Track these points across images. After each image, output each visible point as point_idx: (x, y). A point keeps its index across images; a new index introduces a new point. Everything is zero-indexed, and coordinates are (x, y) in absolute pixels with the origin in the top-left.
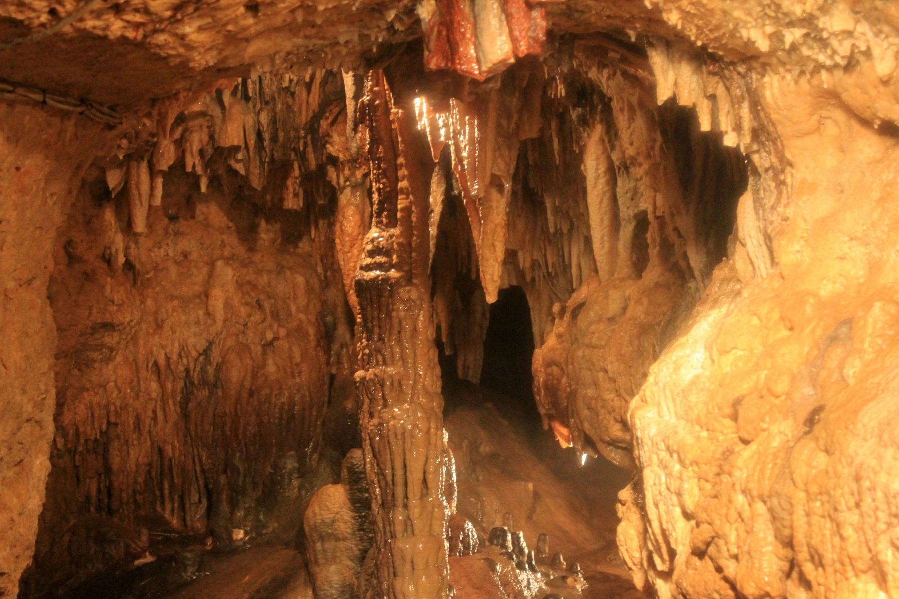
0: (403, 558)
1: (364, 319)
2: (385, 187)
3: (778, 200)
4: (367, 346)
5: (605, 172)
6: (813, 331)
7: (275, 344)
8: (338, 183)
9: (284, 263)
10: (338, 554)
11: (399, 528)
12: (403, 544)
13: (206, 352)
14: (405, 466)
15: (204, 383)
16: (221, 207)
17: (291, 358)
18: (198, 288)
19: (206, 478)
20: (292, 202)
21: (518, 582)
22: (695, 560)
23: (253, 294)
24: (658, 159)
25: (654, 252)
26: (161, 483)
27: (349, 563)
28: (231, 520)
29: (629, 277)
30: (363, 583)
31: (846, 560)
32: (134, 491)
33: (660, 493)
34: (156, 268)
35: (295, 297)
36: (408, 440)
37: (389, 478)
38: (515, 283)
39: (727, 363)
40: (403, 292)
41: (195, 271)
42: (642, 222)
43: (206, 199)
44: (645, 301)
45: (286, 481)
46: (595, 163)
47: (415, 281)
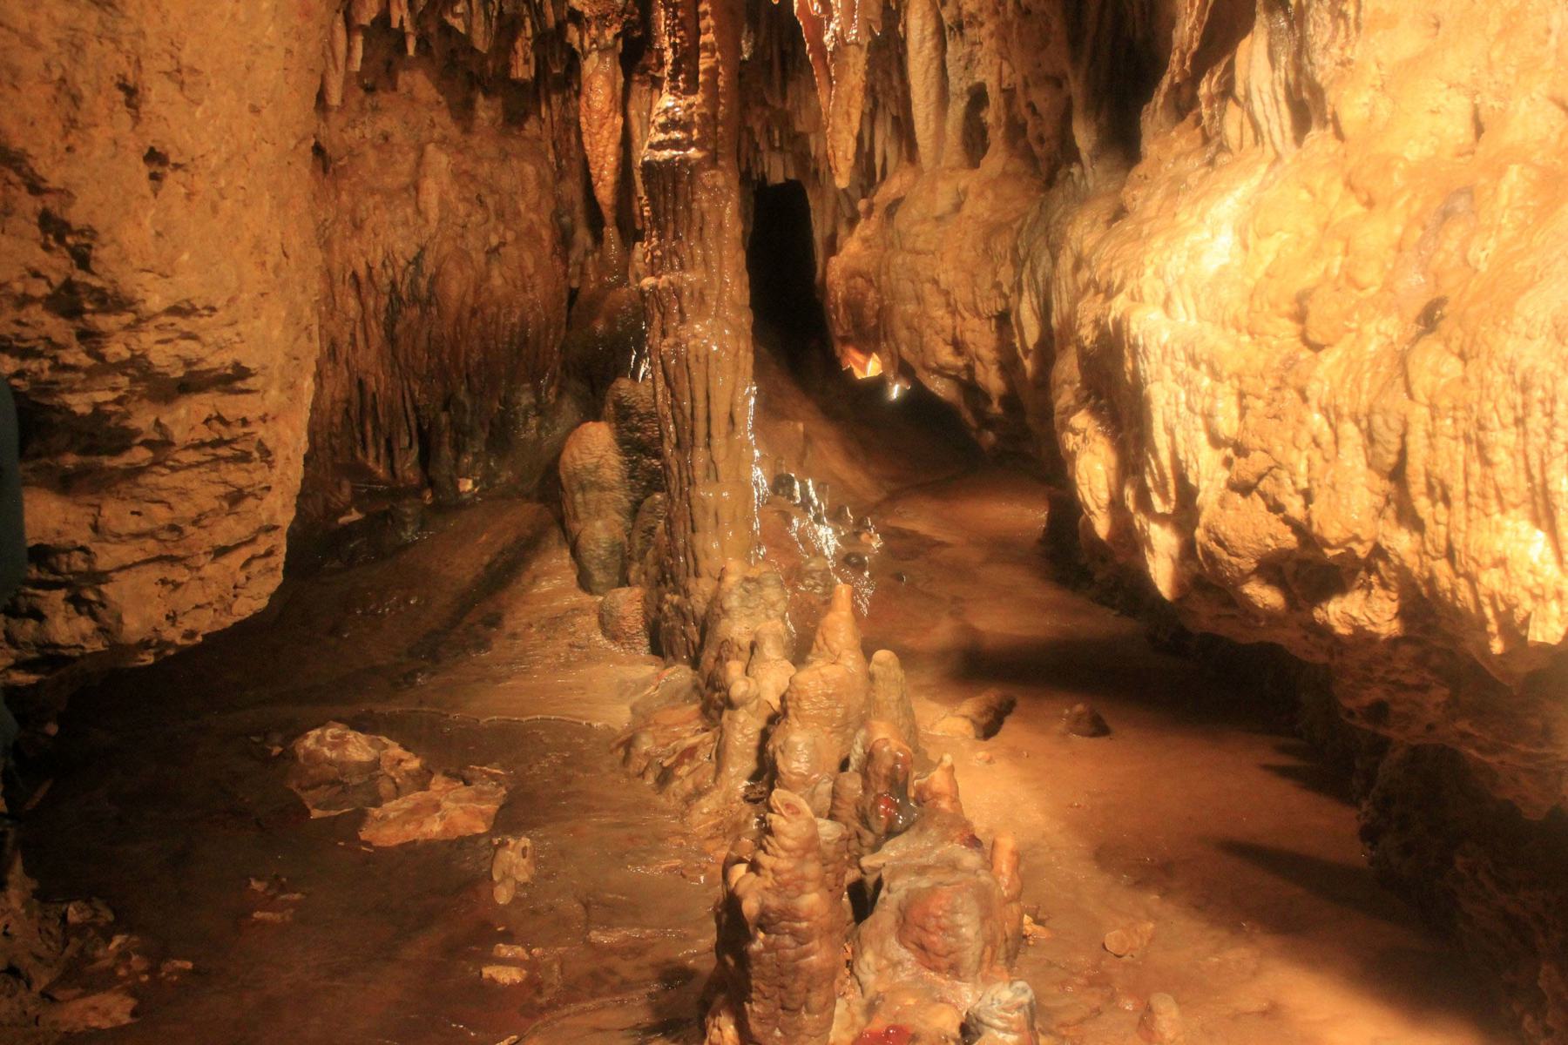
0: (705, 511)
1: (654, 211)
2: (683, 42)
3: (1333, 38)
4: (658, 247)
5: (934, 34)
6: (1408, 204)
7: (502, 250)
8: (582, 46)
9: (508, 148)
10: (604, 506)
11: (699, 473)
12: (705, 493)
13: (417, 261)
14: (708, 397)
15: (415, 299)
16: (428, 75)
17: (522, 268)
18: (405, 180)
19: (418, 418)
20: (522, 71)
21: (819, 538)
22: (1237, 497)
23: (472, 187)
24: (1010, 15)
25: (996, 137)
26: (362, 424)
27: (617, 517)
28: (456, 467)
29: (961, 166)
30: (637, 542)
31: (1491, 492)
32: (330, 435)
33: (1178, 415)
34: (350, 153)
35: (525, 192)
36: (712, 364)
37: (688, 412)
38: (792, 176)
39: (1269, 249)
40: (706, 176)
41: (398, 156)
42: (978, 97)
43: (410, 66)
44: (989, 194)
45: (521, 419)
46: (920, 22)
47: (722, 163)
